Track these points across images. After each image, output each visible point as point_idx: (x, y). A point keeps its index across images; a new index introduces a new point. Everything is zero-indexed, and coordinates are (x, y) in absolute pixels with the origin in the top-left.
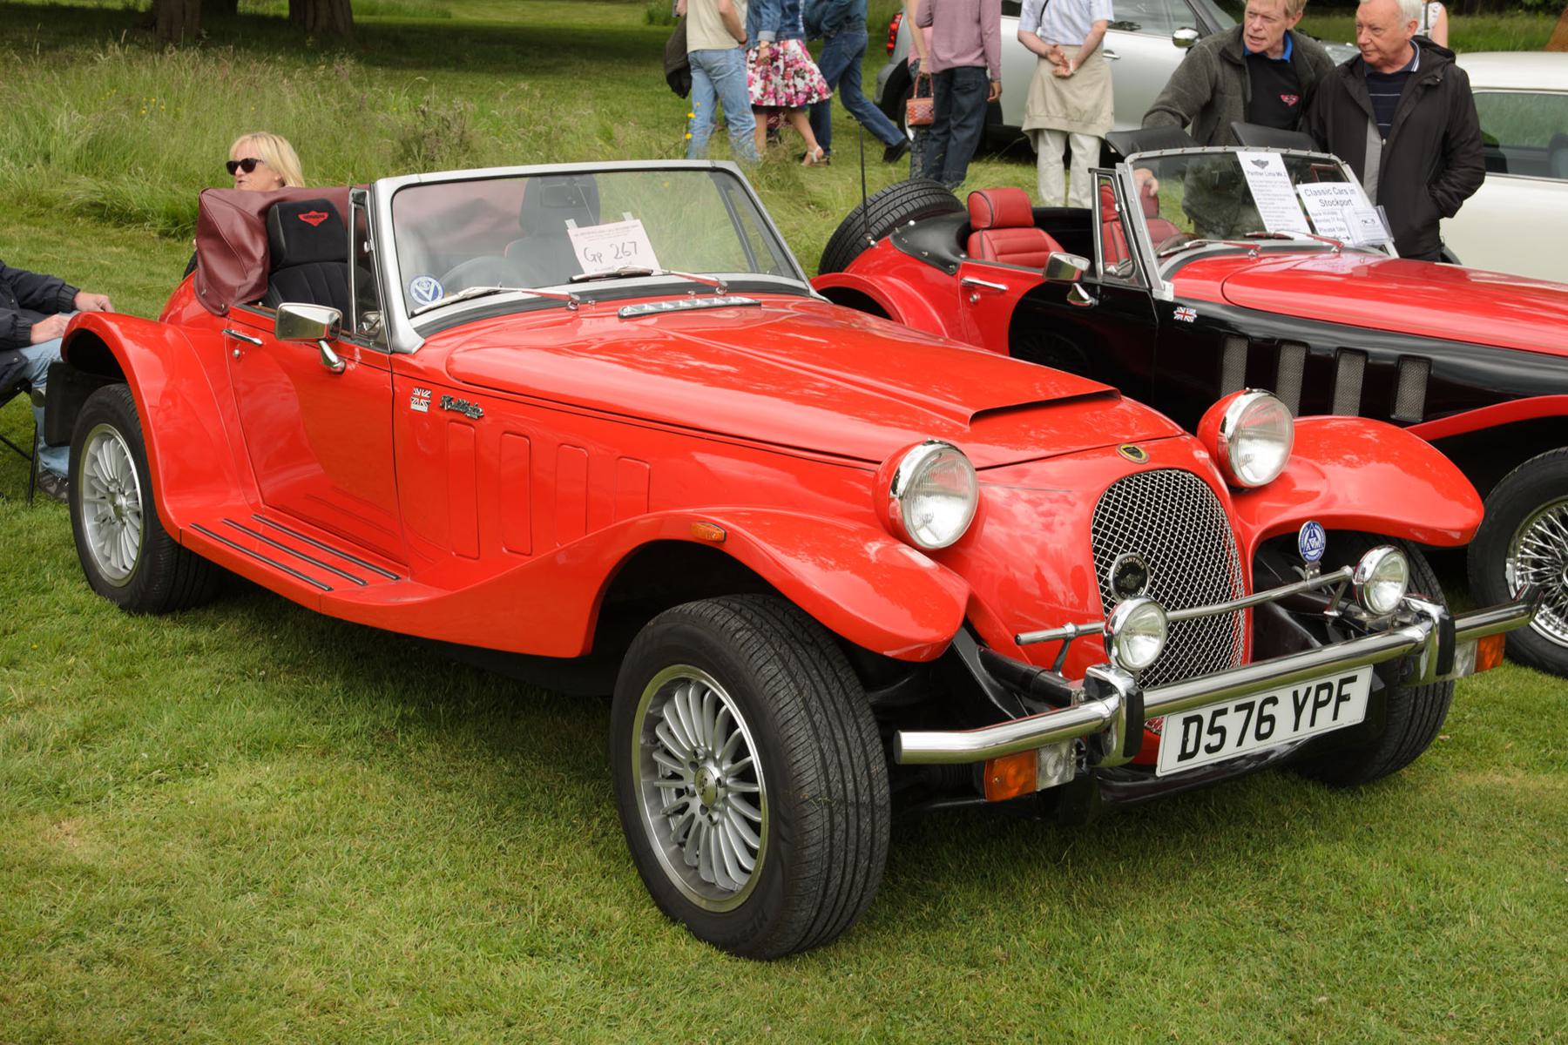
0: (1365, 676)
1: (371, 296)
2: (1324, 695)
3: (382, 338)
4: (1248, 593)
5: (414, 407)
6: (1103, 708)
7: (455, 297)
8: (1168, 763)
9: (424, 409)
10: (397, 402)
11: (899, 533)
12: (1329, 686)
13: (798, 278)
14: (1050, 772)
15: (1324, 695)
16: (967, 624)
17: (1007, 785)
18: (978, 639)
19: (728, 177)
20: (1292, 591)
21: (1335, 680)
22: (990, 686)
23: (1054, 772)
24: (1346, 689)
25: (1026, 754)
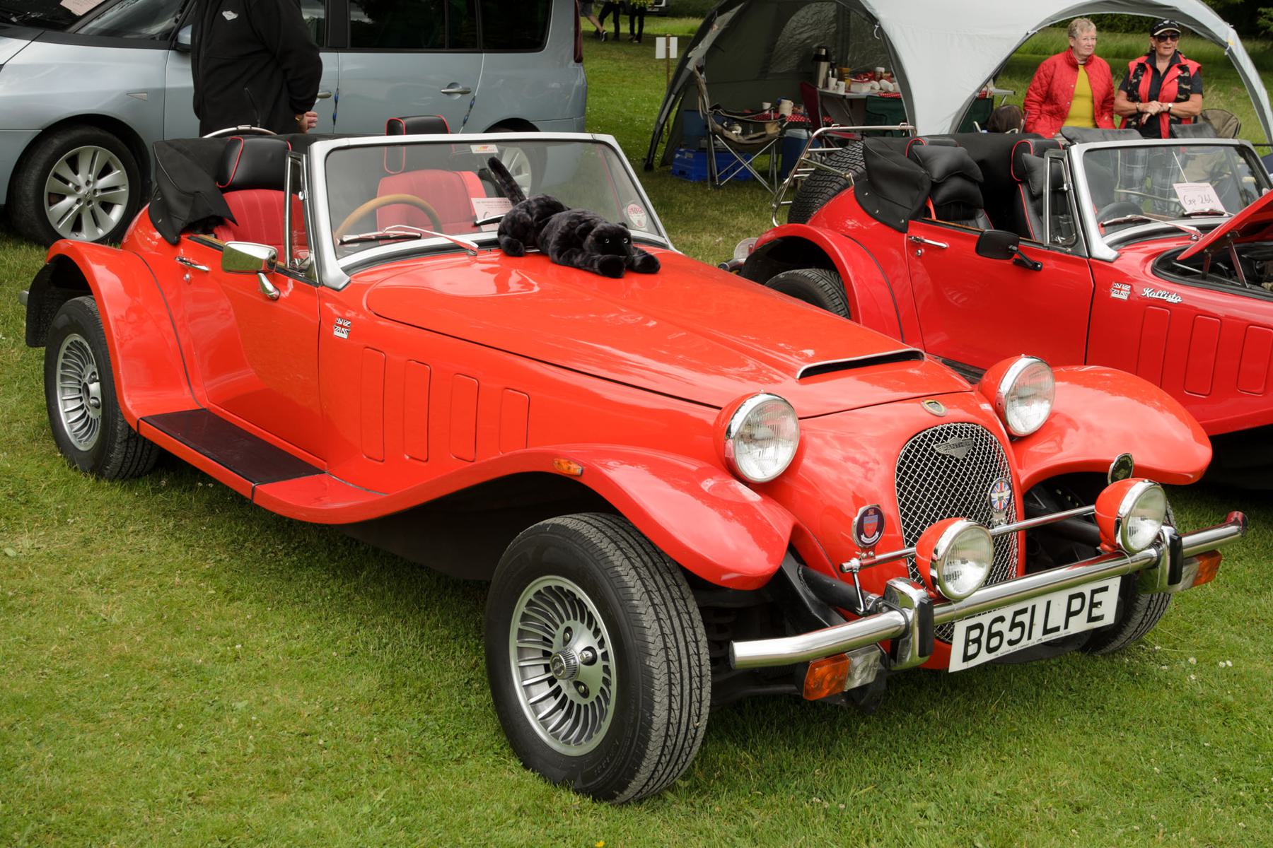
0: (1115, 584)
1: (304, 234)
2: (1076, 604)
3: (310, 277)
4: (1018, 519)
5: (336, 333)
6: (891, 619)
7: (372, 235)
8: (956, 664)
9: (345, 336)
10: (321, 331)
11: (733, 471)
12: (1082, 595)
13: (659, 234)
14: (857, 676)
15: (1076, 604)
16: (792, 549)
17: (820, 684)
18: (799, 559)
19: (604, 147)
20: (1062, 512)
21: (1086, 590)
22: (808, 597)
23: (861, 674)
24: (1097, 598)
25: (837, 656)
